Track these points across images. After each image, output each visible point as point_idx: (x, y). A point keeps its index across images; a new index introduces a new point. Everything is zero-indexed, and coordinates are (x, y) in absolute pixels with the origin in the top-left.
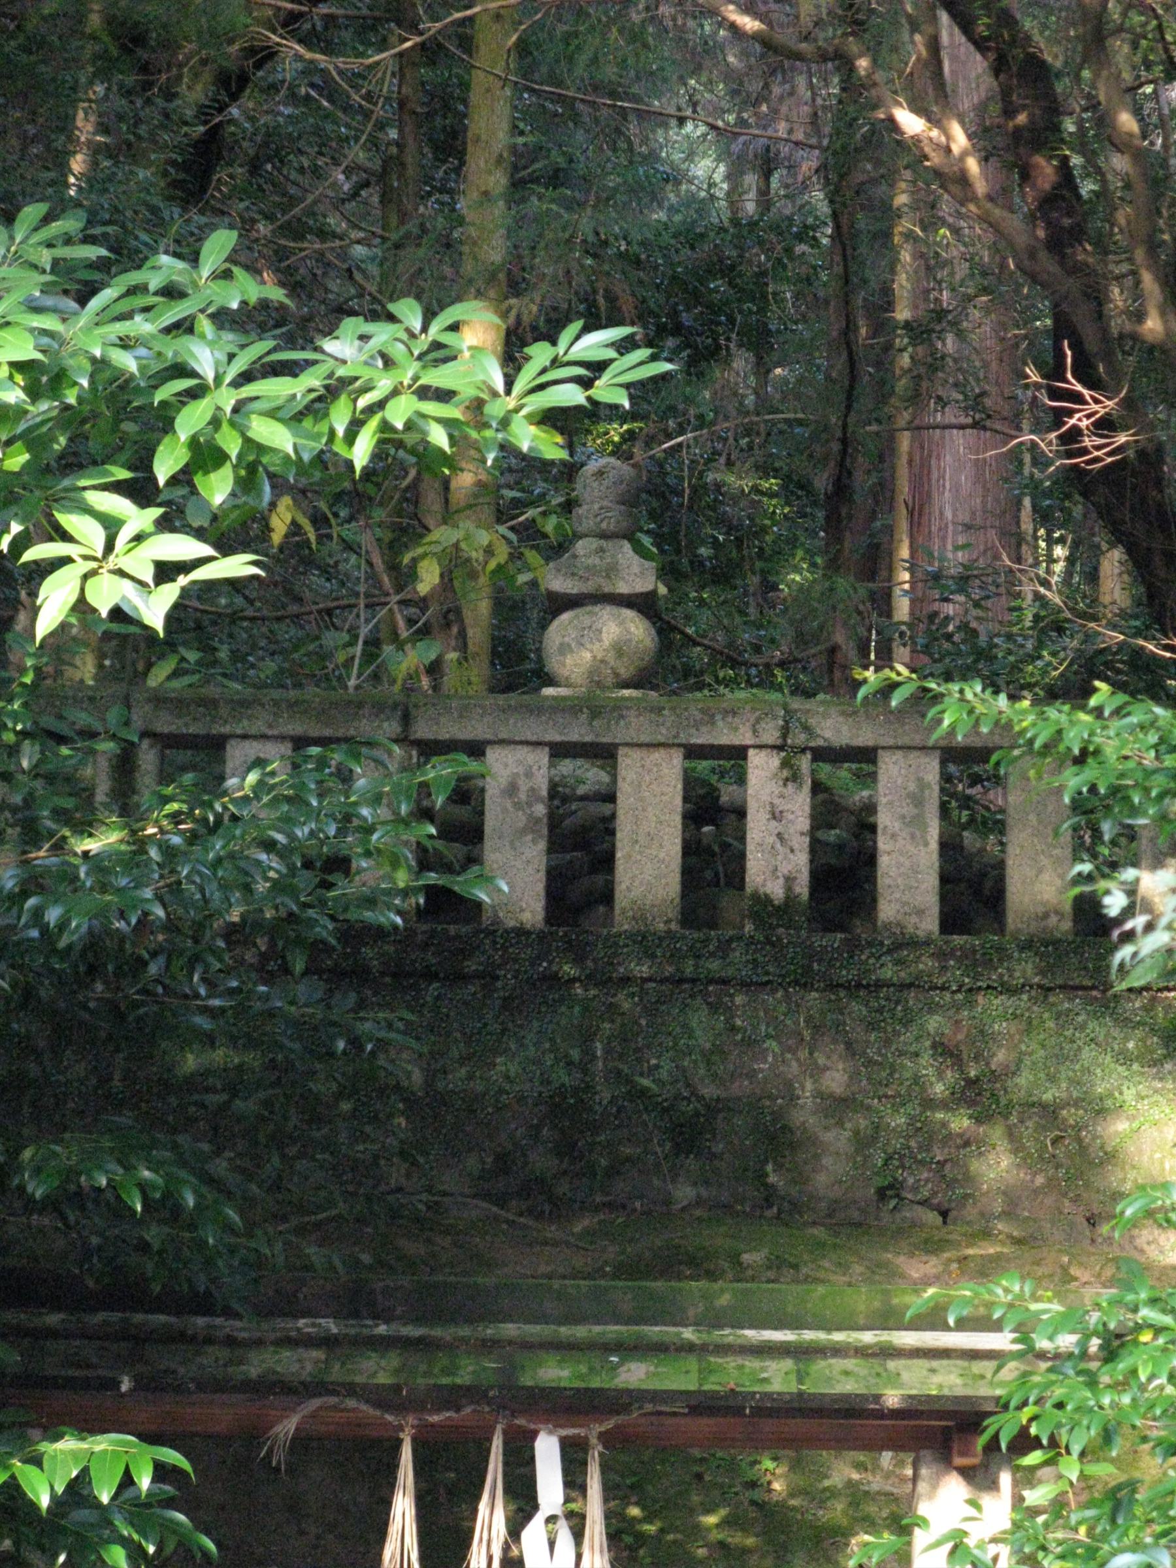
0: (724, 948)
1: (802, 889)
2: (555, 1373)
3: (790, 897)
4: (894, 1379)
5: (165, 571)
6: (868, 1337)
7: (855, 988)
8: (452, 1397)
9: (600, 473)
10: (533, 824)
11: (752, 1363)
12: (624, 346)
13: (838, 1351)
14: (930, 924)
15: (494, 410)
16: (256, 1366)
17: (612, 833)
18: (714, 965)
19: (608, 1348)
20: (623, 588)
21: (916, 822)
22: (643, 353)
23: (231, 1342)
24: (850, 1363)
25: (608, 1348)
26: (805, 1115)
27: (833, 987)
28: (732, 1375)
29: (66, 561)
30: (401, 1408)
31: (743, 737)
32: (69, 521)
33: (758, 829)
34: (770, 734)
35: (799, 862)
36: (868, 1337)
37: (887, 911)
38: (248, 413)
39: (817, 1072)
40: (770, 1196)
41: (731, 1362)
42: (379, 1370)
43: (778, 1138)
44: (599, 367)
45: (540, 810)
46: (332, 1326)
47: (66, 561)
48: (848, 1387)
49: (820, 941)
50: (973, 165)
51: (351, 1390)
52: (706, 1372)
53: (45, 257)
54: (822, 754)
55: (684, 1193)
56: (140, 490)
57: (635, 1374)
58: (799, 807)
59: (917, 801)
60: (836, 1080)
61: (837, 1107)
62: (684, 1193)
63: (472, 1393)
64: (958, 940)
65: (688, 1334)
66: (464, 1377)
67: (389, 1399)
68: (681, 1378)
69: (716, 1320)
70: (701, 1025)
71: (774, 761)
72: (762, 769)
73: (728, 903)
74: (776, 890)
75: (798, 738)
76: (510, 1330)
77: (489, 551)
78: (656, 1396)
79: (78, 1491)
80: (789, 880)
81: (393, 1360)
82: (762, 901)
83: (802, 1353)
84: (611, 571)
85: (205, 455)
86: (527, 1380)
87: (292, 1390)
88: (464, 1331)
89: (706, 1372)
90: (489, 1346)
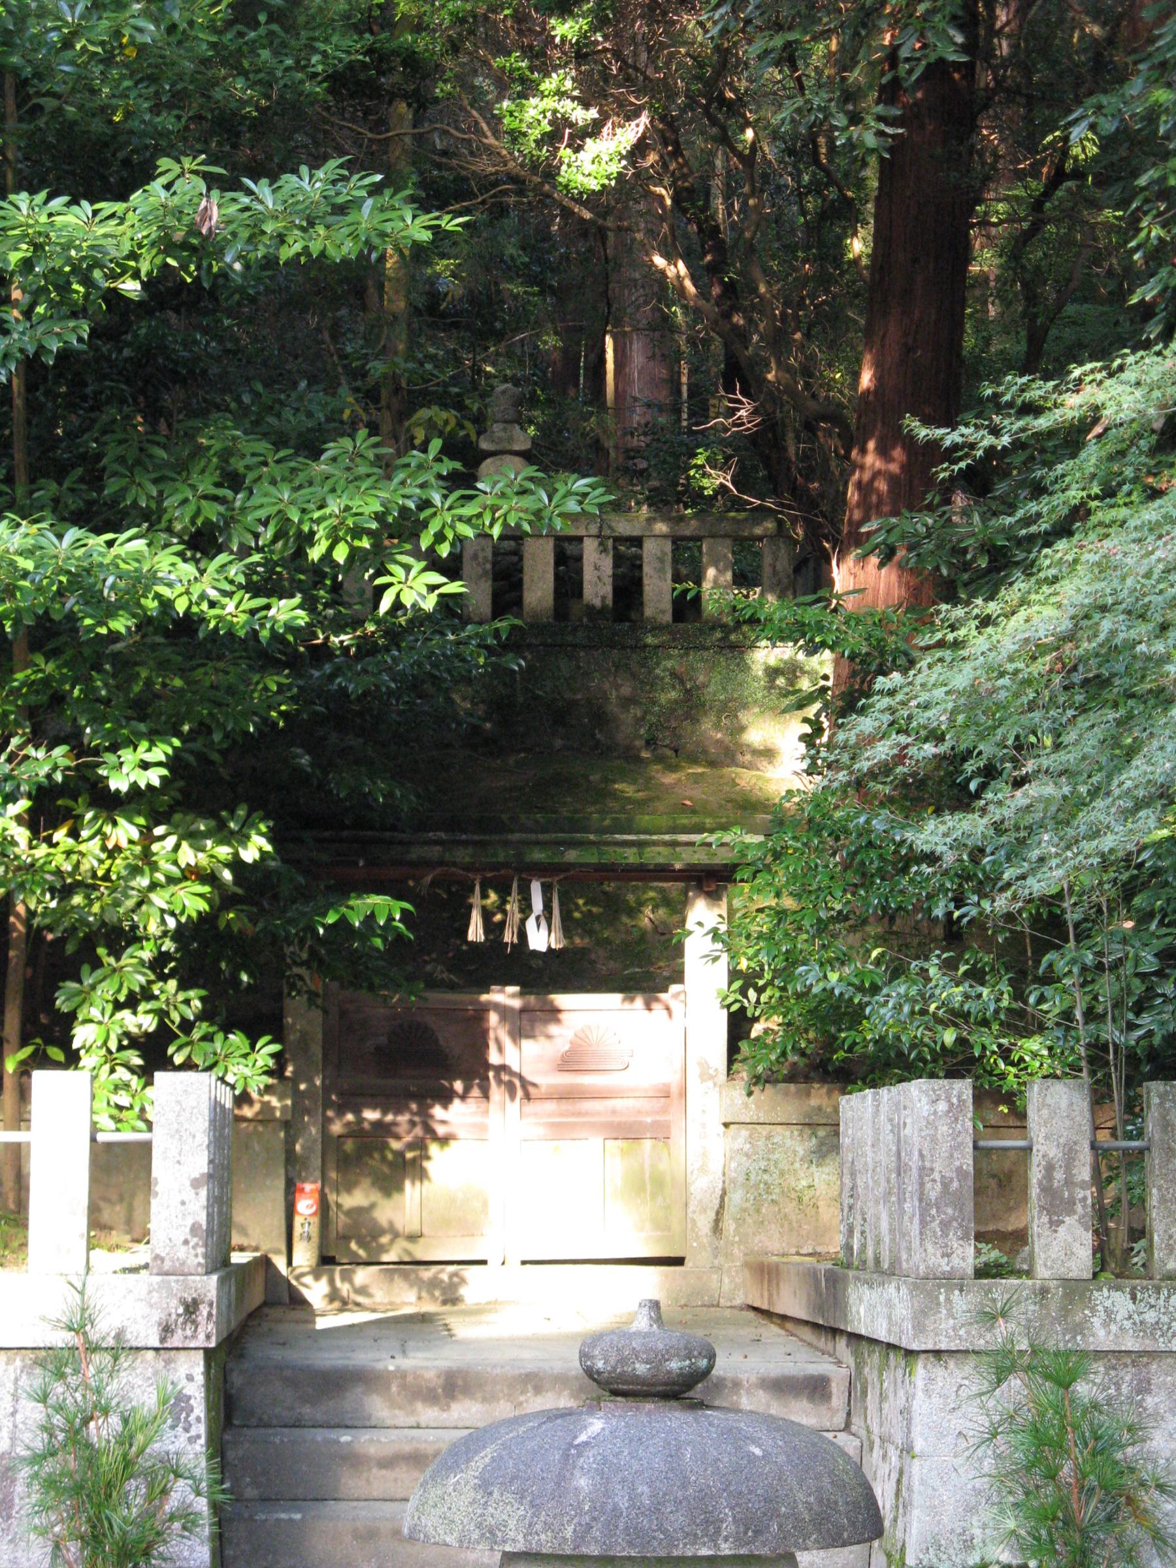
0: (575, 629)
1: (609, 601)
2: (539, 856)
3: (604, 607)
4: (678, 859)
5: (432, 588)
6: (667, 837)
7: (634, 648)
8: (496, 867)
9: (504, 392)
10: (485, 573)
11: (619, 850)
12: (593, 487)
13: (655, 843)
14: (668, 617)
15: (546, 514)
16: (415, 853)
17: (521, 571)
18: (570, 638)
19: (558, 843)
20: (516, 448)
21: (661, 570)
22: (601, 490)
23: (401, 843)
24: (660, 849)
25: (558, 843)
26: (613, 707)
27: (624, 648)
28: (613, 855)
29: (391, 585)
30: (477, 870)
31: (581, 532)
32: (393, 568)
33: (589, 574)
34: (594, 530)
35: (608, 590)
36: (667, 837)
37: (648, 612)
38: (453, 522)
39: (618, 687)
40: (597, 744)
41: (611, 849)
42: (463, 855)
43: (600, 718)
44: (585, 495)
45: (489, 566)
46: (443, 835)
47: (391, 585)
48: (661, 860)
49: (618, 627)
50: (688, 283)
51: (455, 864)
52: (601, 854)
53: (370, 454)
54: (618, 540)
55: (558, 743)
56: (417, 554)
57: (572, 856)
58: (607, 563)
59: (661, 560)
60: (626, 690)
61: (627, 702)
62: (558, 743)
63: (506, 865)
64: (681, 625)
65: (592, 837)
66: (501, 858)
67: (468, 868)
68: (591, 857)
69: (602, 831)
70: (565, 667)
71: (596, 542)
72: (590, 548)
73: (575, 608)
74: (597, 603)
75: (606, 532)
76: (516, 836)
77: (446, 422)
78: (582, 865)
79: (371, 918)
80: (604, 598)
81: (470, 850)
82: (590, 608)
83: (640, 845)
84: (511, 439)
85: (440, 537)
86: (528, 859)
87: (429, 864)
88: (496, 837)
89: (601, 854)
90: (506, 844)
